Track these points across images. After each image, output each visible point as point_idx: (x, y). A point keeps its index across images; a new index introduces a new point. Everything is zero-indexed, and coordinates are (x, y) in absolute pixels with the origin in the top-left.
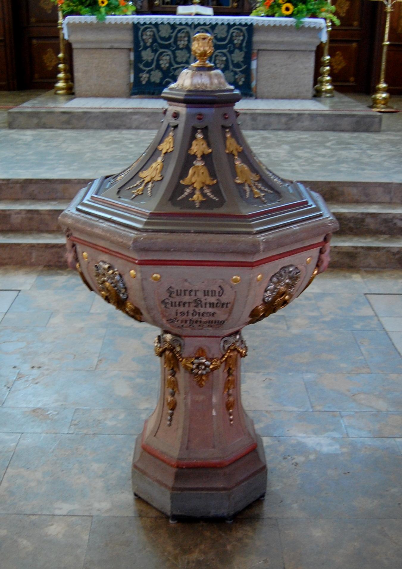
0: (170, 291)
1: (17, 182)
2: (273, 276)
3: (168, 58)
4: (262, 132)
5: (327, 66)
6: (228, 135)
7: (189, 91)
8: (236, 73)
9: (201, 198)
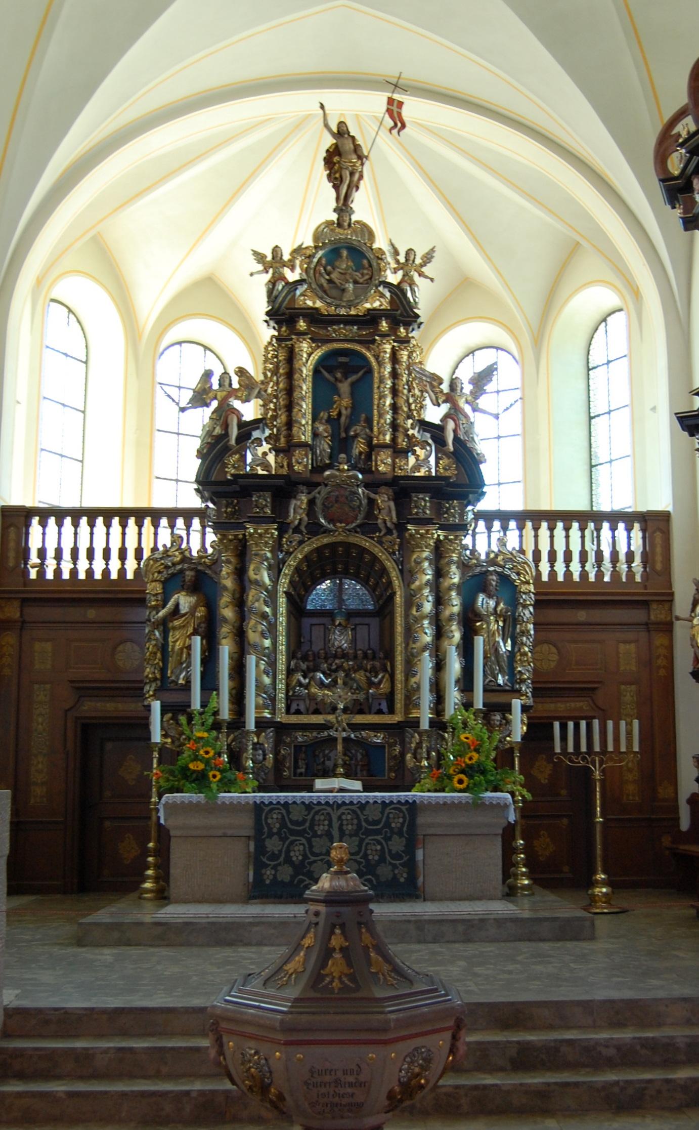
0: (312, 1072)
1: (104, 1011)
2: (406, 1056)
3: (301, 848)
4: (431, 946)
5: (521, 853)
6: (364, 930)
7: (328, 892)
8: (395, 867)
9: (339, 985)
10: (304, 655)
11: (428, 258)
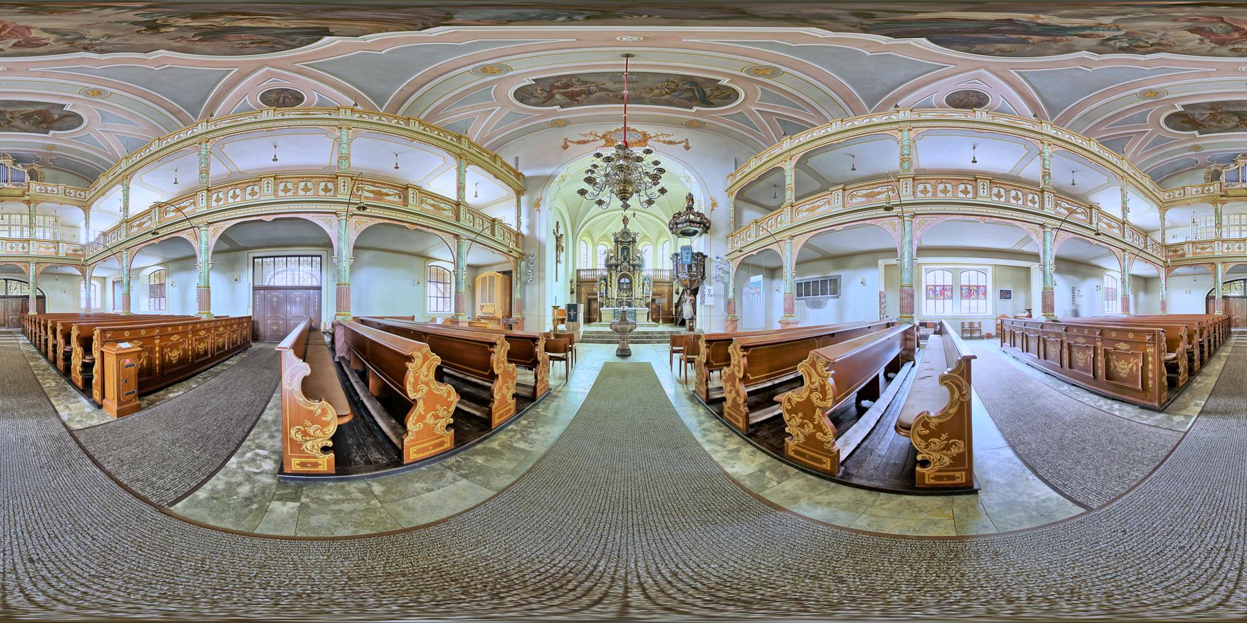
10: (620, 289)
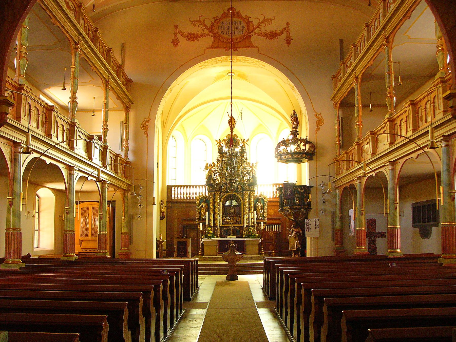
11: (248, 140)
